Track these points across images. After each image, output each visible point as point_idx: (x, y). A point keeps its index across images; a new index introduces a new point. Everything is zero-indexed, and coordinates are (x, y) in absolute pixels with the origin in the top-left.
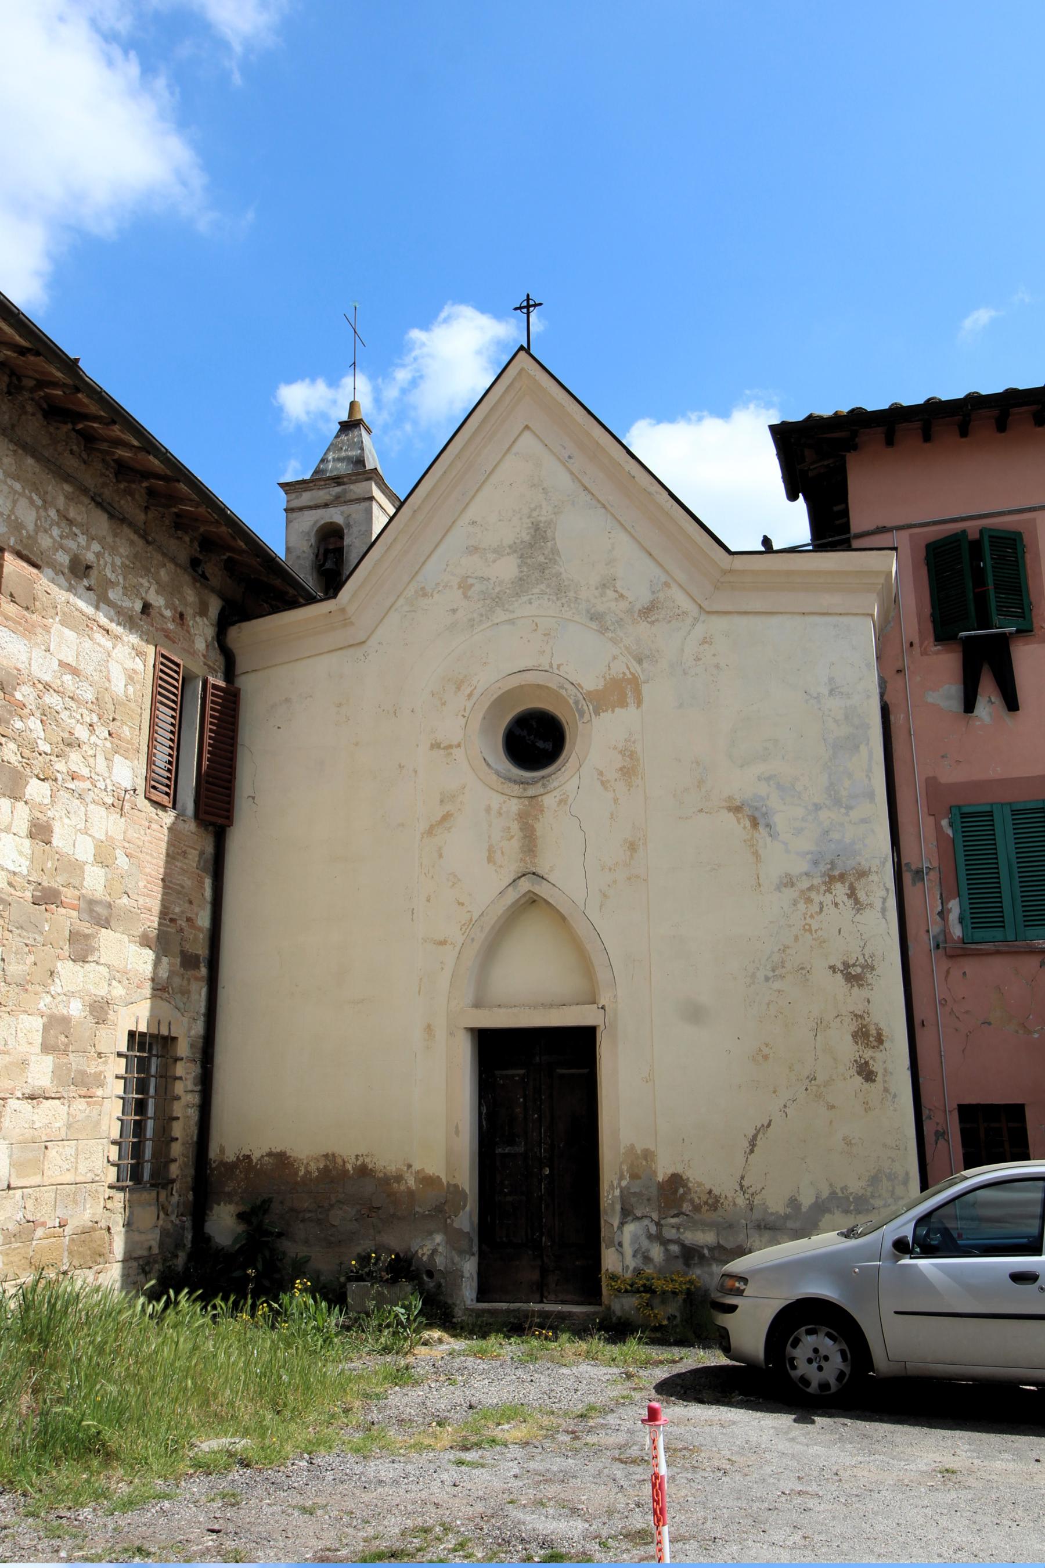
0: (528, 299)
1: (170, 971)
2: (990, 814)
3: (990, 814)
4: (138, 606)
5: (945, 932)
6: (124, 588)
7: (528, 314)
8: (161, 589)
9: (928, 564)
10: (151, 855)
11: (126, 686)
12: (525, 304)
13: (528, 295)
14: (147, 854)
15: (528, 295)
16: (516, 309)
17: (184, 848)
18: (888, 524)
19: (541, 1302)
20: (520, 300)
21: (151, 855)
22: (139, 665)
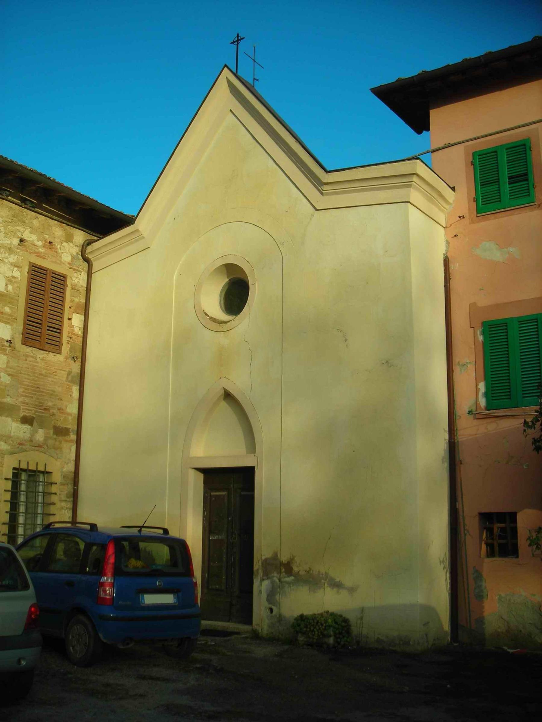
0: (238, 36)
1: (45, 437)
2: (506, 325)
3: (506, 325)
4: (16, 241)
5: (477, 403)
6: (5, 233)
7: (237, 45)
8: (33, 231)
9: (120, 213)
10: (28, 375)
11: (6, 285)
12: (236, 39)
13: (238, 34)
14: (25, 374)
15: (238, 34)
16: (231, 43)
17: (55, 370)
18: (452, 143)
19: (228, 621)
20: (233, 37)
21: (28, 375)
22: (17, 273)
